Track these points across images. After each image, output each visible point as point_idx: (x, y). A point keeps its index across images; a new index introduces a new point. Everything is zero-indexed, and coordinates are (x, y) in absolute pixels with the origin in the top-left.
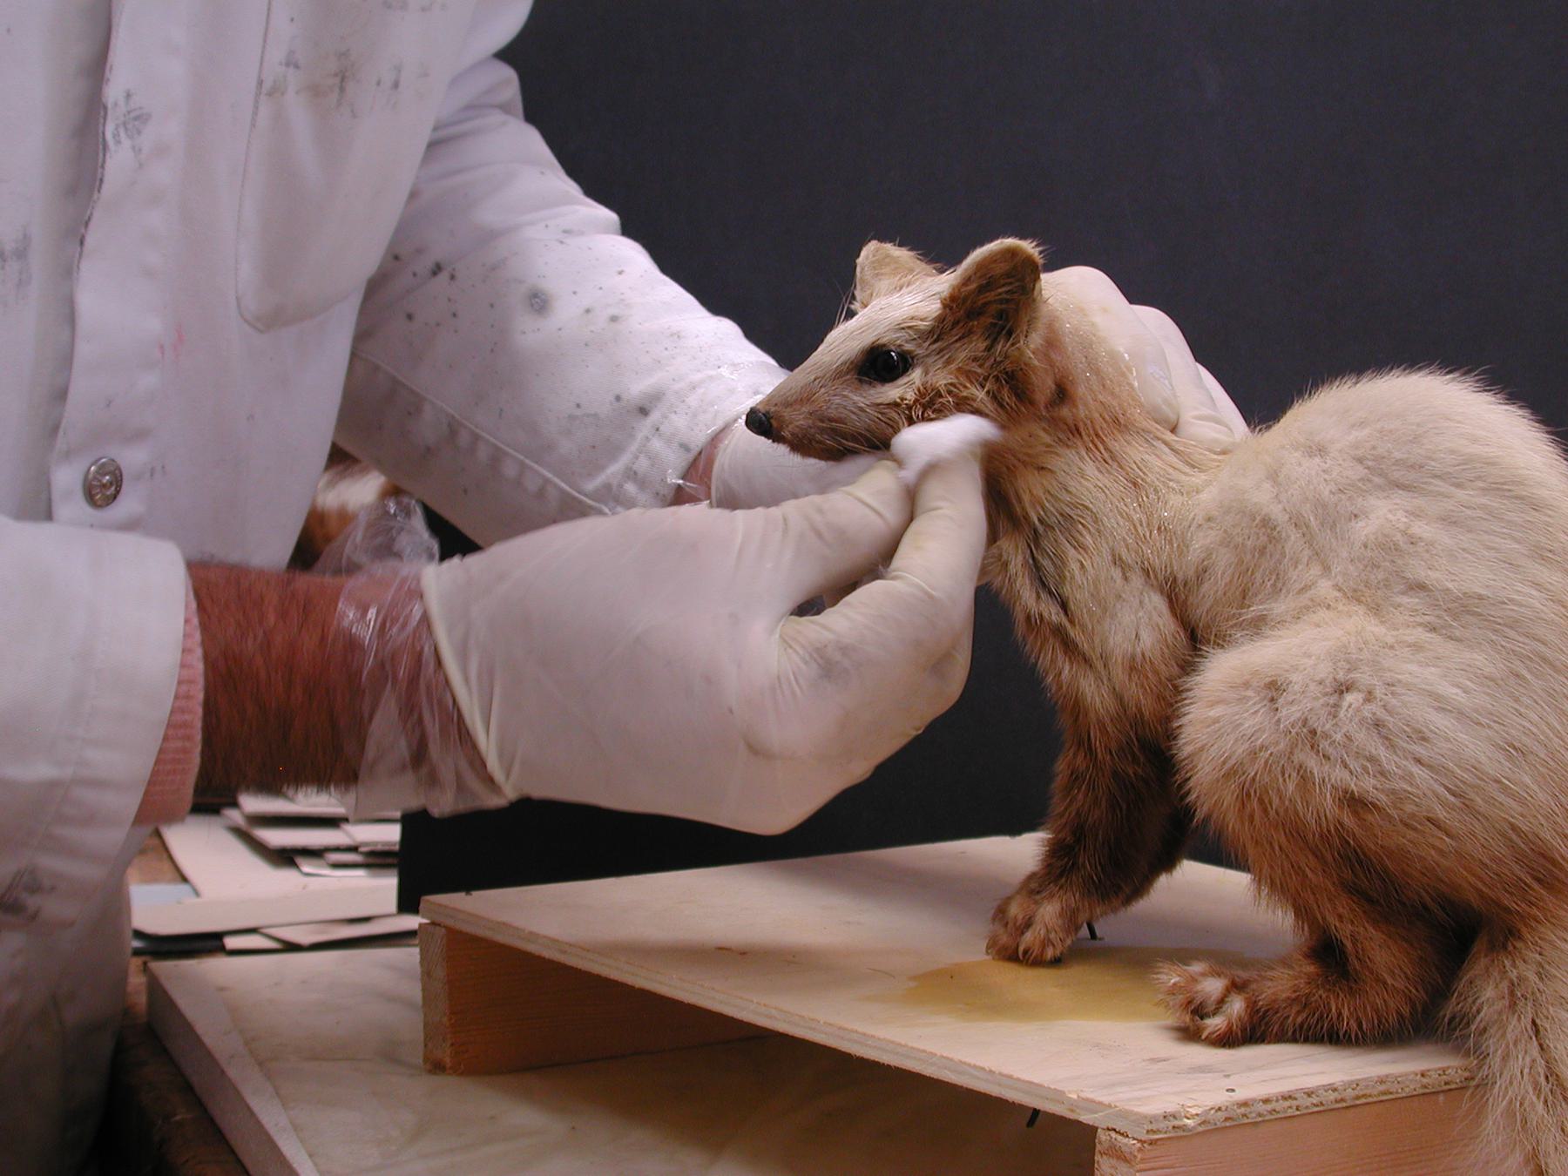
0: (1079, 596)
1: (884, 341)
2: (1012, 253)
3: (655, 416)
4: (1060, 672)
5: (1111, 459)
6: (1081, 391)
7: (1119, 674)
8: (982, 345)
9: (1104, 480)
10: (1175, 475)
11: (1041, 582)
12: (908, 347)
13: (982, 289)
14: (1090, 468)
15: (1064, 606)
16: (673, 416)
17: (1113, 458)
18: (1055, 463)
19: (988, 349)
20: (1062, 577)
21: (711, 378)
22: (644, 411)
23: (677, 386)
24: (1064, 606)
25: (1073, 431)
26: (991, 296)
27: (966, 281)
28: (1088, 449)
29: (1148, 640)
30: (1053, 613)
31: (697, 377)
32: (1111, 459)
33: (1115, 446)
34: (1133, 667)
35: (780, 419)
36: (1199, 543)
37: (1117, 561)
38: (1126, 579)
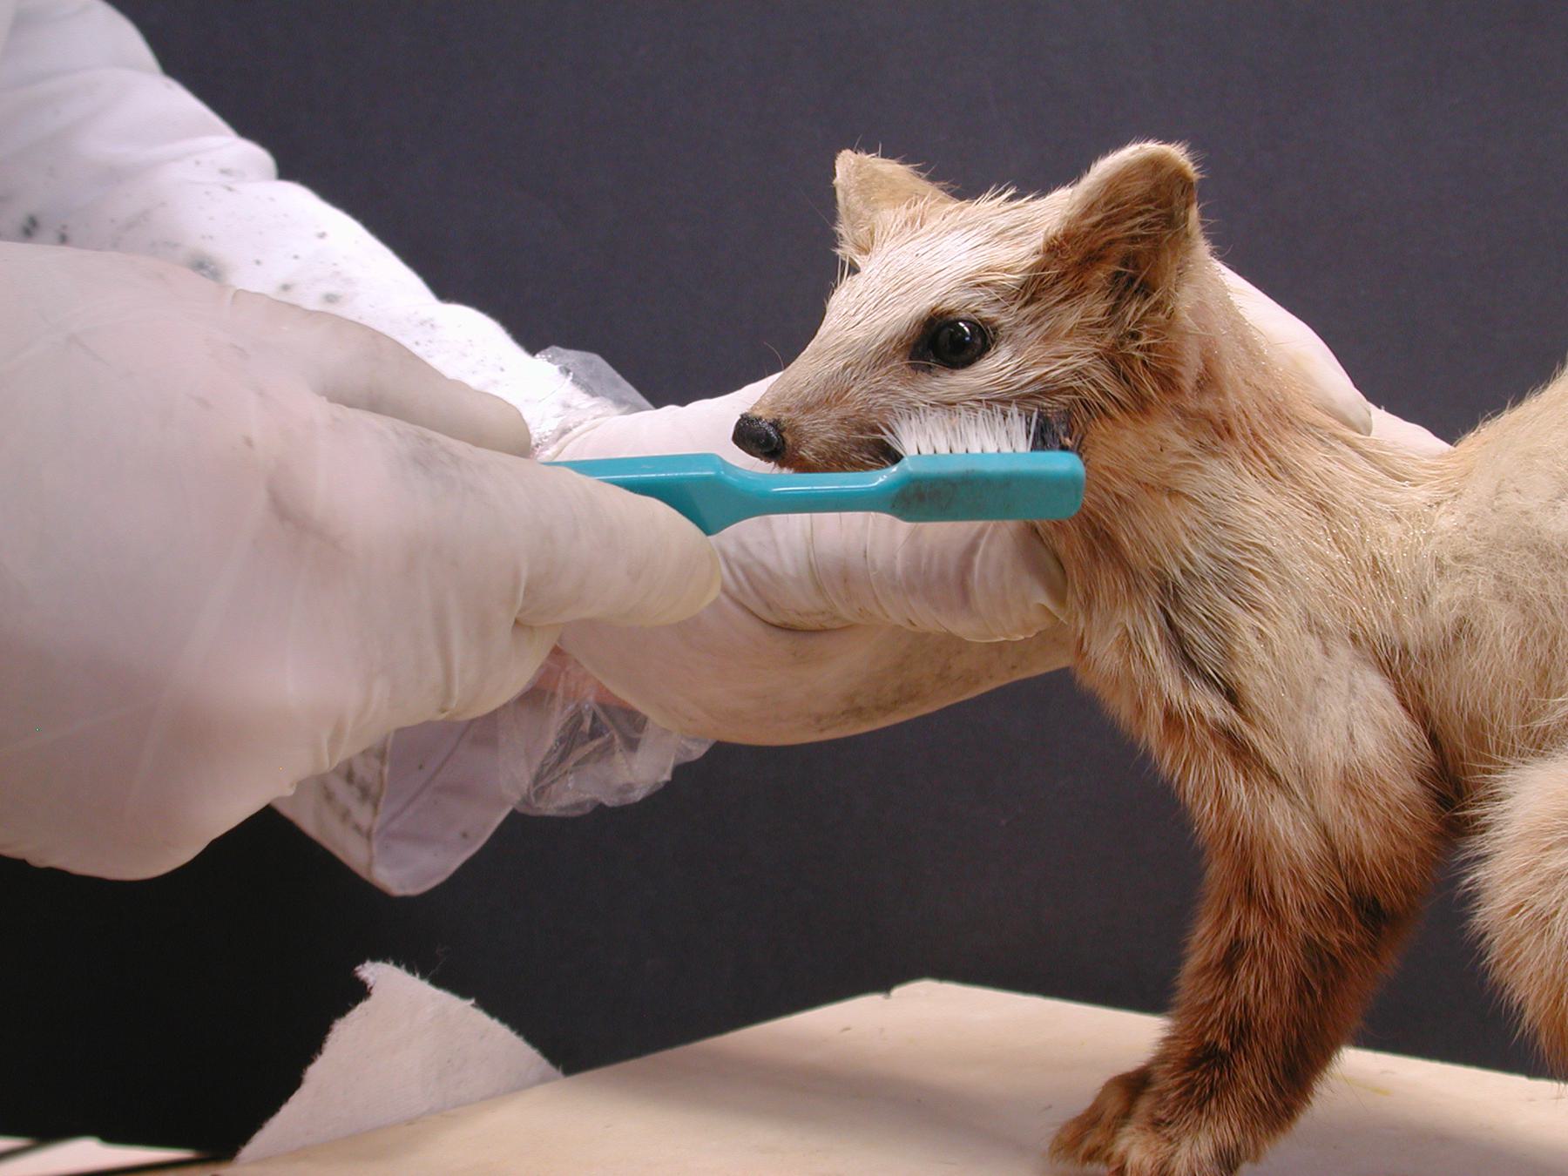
0: (1257, 684)
1: (951, 304)
2: (1155, 165)
4: (1211, 790)
5: (1281, 472)
7: (1330, 799)
8: (1101, 307)
9: (1278, 504)
10: (1376, 491)
11: (1188, 660)
12: (987, 313)
13: (1110, 221)
14: (1253, 488)
15: (1233, 696)
17: (1284, 468)
18: (1194, 484)
19: (1112, 311)
20: (1228, 654)
24: (1233, 696)
25: (1218, 431)
26: (1119, 231)
27: (1089, 209)
28: (1244, 457)
29: (1369, 743)
30: (1213, 706)
32: (1281, 472)
34: (1349, 783)
35: (794, 429)
36: (1446, 597)
37: (1314, 626)
38: (1326, 652)
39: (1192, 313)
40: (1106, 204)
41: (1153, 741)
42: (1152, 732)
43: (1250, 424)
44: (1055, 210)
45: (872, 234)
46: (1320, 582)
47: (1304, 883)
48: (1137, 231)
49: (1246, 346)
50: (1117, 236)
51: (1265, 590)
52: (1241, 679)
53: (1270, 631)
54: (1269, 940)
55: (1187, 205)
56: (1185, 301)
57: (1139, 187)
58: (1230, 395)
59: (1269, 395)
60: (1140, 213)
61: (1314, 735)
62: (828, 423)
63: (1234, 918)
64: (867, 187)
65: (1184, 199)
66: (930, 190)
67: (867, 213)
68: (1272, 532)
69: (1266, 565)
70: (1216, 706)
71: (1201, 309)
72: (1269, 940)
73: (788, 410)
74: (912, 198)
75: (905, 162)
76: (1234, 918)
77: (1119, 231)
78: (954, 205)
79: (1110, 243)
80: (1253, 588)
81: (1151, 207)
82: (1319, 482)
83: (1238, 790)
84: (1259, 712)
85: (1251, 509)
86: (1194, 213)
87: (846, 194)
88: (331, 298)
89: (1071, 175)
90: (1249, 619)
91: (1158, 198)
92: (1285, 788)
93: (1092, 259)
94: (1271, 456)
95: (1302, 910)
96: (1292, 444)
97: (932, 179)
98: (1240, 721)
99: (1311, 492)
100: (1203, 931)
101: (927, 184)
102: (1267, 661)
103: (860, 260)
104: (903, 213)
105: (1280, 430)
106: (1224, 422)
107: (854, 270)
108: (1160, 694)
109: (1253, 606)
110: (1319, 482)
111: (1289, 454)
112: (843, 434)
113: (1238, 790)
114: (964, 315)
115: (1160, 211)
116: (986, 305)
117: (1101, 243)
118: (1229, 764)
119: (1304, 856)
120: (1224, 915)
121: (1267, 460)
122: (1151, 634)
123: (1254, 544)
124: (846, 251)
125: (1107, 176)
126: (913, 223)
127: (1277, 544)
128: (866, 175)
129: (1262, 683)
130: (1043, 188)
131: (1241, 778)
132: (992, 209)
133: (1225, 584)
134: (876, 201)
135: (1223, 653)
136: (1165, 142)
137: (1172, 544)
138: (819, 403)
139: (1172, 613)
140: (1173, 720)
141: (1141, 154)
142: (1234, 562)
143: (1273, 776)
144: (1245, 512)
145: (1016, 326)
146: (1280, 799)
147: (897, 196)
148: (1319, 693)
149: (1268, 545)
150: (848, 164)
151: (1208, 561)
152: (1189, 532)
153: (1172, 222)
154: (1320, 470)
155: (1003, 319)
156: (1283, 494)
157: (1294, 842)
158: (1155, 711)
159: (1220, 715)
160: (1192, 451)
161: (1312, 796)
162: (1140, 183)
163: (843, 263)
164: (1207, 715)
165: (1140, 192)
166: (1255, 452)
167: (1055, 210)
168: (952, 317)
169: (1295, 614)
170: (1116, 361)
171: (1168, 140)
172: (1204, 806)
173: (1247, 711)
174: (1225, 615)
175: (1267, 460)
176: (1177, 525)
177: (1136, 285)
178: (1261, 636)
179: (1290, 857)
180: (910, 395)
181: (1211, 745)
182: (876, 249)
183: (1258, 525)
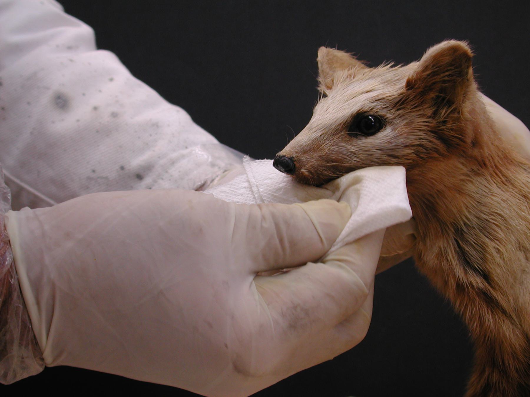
1: (366, 109)
2: (454, 50)
3: (148, 180)
6: (485, 138)
9: (506, 196)
11: (466, 261)
12: (381, 113)
13: (434, 74)
14: (495, 189)
16: (160, 181)
18: (470, 188)
20: (484, 259)
21: (183, 156)
22: (139, 177)
23: (162, 162)
24: (486, 276)
25: (480, 165)
26: (438, 78)
27: (426, 68)
30: (477, 281)
31: (174, 155)
33: (509, 174)
35: (299, 161)
39: (470, 113)
40: (433, 66)
41: (451, 296)
42: (451, 294)
43: (494, 162)
44: (413, 68)
45: (333, 81)
46: (524, 228)
47: (517, 358)
48: (446, 78)
49: (492, 129)
50: (437, 80)
51: (500, 232)
52: (490, 270)
53: (502, 249)
54: (502, 383)
55: (468, 67)
56: (467, 107)
57: (447, 59)
58: (486, 150)
59: (502, 150)
60: (448, 71)
61: (522, 294)
62: (313, 158)
63: (487, 374)
64: (331, 62)
65: (466, 65)
66: (358, 64)
67: (331, 73)
68: (504, 207)
69: (501, 222)
70: (479, 281)
71: (473, 111)
72: (502, 383)
73: (297, 153)
74: (350, 67)
75: (347, 52)
76: (487, 374)
77: (438, 78)
78: (367, 70)
79: (434, 83)
80: (495, 231)
81: (452, 68)
82: (523, 186)
83: (489, 318)
84: (498, 284)
85: (494, 198)
86: (471, 71)
87: (322, 65)
88: (114, 115)
89: (418, 58)
90: (493, 244)
91: (455, 62)
92: (510, 317)
93: (423, 94)
94: (503, 175)
95: (517, 371)
96: (512, 170)
97: (359, 59)
98: (489, 288)
99: (520, 191)
100: (473, 379)
101: (357, 61)
102: (501, 262)
103: (327, 92)
104: (346, 73)
105: (507, 164)
106: (483, 160)
107: (325, 96)
108: (454, 276)
109: (495, 239)
110: (523, 186)
111: (511, 175)
112: (320, 163)
113: (489, 318)
114: (371, 113)
115: (456, 70)
116: (382, 109)
117: (430, 83)
118: (484, 306)
119: (518, 347)
120: (483, 371)
121: (501, 176)
122: (451, 250)
123: (496, 213)
124: (322, 88)
125: (433, 54)
126: (350, 76)
127: (506, 213)
128: (331, 57)
129: (499, 271)
130: (406, 62)
131: (490, 312)
132: (384, 71)
133: (483, 229)
134: (335, 68)
135: (482, 259)
136: (459, 40)
137: (460, 211)
138: (310, 150)
139: (460, 242)
140: (460, 287)
141: (449, 45)
142: (487, 220)
143: (504, 312)
144: (492, 199)
145: (394, 118)
146: (507, 322)
147: (343, 66)
148: (524, 276)
149: (503, 214)
150: (323, 53)
151: (475, 219)
152: (467, 208)
153: (461, 74)
154: (524, 181)
155: (388, 115)
156: (508, 191)
157: (513, 340)
158: (452, 283)
159: (481, 285)
160: (469, 173)
161: (521, 321)
162: (447, 58)
163: (321, 93)
164: (475, 284)
165: (447, 61)
166: (496, 174)
167: (413, 68)
168: (366, 114)
169: (513, 242)
170: (436, 132)
171: (460, 39)
172: (474, 324)
173: (493, 283)
174: (483, 242)
175: (501, 176)
176: (462, 205)
177: (445, 102)
178: (499, 251)
179: (511, 347)
180: (348, 147)
181: (477, 299)
182: (334, 87)
183: (498, 205)
